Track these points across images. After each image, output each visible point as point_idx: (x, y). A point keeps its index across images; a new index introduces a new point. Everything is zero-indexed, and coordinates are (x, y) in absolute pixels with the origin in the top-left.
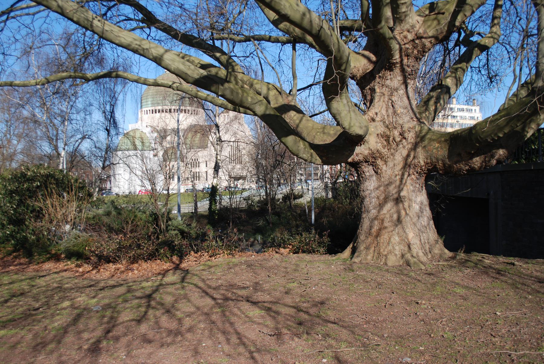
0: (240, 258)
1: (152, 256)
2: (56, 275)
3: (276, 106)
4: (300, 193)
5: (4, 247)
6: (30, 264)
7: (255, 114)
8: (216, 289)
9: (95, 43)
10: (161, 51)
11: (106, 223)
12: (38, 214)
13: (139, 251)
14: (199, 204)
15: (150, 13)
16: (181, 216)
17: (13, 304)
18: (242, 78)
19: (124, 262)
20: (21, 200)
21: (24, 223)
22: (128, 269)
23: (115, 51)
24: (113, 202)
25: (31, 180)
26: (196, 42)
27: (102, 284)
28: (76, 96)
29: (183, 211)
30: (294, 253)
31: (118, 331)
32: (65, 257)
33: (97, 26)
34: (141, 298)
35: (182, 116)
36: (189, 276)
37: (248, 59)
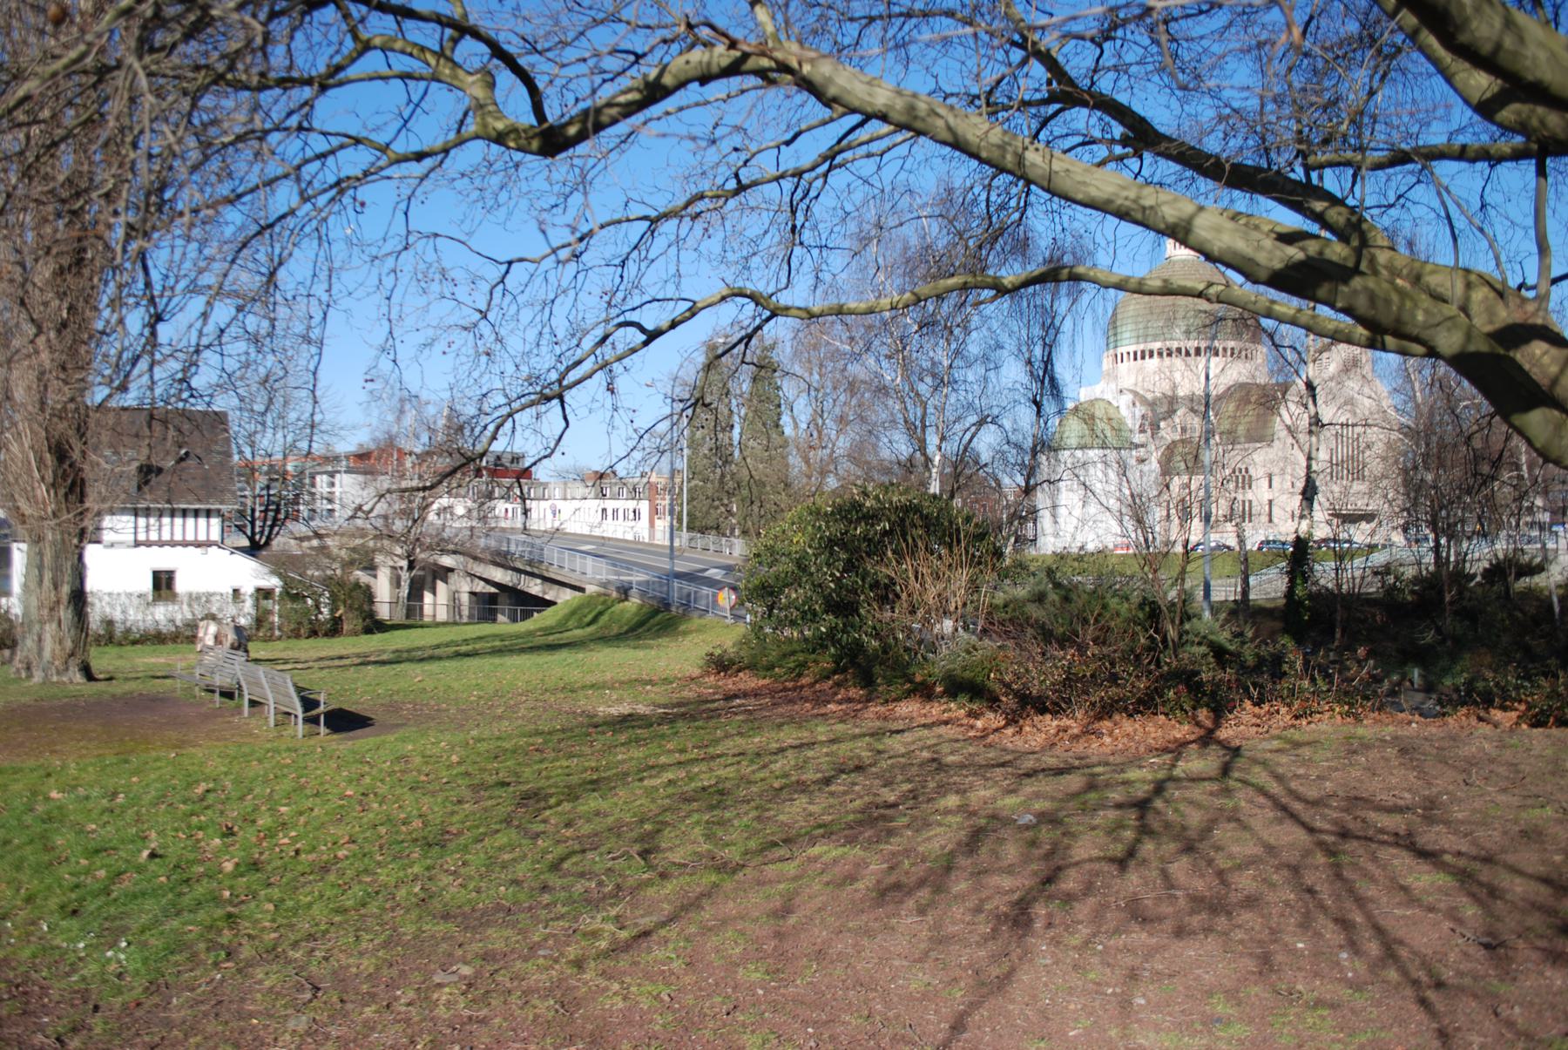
0: (1377, 729)
1: (1146, 705)
2: (926, 732)
3: (1488, 328)
4: (1538, 560)
5: (815, 661)
6: (869, 701)
7: (1432, 353)
8: (1314, 803)
9: (1013, 203)
10: (1188, 208)
11: (1037, 621)
12: (886, 594)
13: (1113, 691)
14: (1252, 581)
15: (1143, 120)
16: (1212, 608)
17: (841, 788)
18: (1391, 260)
19: (1079, 715)
20: (849, 561)
21: (857, 611)
22: (1086, 732)
23: (1057, 219)
24: (1050, 572)
25: (872, 517)
26: (1264, 180)
27: (1029, 764)
28: (965, 328)
29: (1217, 596)
30: (1533, 726)
31: (1070, 882)
32: (944, 692)
33: (1034, 165)
34: (1119, 806)
35: (1216, 363)
36: (1240, 762)
37: (1392, 212)
